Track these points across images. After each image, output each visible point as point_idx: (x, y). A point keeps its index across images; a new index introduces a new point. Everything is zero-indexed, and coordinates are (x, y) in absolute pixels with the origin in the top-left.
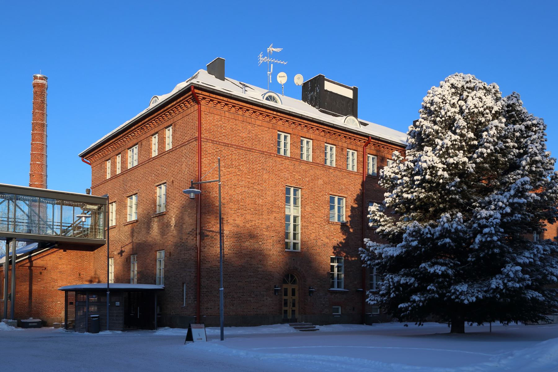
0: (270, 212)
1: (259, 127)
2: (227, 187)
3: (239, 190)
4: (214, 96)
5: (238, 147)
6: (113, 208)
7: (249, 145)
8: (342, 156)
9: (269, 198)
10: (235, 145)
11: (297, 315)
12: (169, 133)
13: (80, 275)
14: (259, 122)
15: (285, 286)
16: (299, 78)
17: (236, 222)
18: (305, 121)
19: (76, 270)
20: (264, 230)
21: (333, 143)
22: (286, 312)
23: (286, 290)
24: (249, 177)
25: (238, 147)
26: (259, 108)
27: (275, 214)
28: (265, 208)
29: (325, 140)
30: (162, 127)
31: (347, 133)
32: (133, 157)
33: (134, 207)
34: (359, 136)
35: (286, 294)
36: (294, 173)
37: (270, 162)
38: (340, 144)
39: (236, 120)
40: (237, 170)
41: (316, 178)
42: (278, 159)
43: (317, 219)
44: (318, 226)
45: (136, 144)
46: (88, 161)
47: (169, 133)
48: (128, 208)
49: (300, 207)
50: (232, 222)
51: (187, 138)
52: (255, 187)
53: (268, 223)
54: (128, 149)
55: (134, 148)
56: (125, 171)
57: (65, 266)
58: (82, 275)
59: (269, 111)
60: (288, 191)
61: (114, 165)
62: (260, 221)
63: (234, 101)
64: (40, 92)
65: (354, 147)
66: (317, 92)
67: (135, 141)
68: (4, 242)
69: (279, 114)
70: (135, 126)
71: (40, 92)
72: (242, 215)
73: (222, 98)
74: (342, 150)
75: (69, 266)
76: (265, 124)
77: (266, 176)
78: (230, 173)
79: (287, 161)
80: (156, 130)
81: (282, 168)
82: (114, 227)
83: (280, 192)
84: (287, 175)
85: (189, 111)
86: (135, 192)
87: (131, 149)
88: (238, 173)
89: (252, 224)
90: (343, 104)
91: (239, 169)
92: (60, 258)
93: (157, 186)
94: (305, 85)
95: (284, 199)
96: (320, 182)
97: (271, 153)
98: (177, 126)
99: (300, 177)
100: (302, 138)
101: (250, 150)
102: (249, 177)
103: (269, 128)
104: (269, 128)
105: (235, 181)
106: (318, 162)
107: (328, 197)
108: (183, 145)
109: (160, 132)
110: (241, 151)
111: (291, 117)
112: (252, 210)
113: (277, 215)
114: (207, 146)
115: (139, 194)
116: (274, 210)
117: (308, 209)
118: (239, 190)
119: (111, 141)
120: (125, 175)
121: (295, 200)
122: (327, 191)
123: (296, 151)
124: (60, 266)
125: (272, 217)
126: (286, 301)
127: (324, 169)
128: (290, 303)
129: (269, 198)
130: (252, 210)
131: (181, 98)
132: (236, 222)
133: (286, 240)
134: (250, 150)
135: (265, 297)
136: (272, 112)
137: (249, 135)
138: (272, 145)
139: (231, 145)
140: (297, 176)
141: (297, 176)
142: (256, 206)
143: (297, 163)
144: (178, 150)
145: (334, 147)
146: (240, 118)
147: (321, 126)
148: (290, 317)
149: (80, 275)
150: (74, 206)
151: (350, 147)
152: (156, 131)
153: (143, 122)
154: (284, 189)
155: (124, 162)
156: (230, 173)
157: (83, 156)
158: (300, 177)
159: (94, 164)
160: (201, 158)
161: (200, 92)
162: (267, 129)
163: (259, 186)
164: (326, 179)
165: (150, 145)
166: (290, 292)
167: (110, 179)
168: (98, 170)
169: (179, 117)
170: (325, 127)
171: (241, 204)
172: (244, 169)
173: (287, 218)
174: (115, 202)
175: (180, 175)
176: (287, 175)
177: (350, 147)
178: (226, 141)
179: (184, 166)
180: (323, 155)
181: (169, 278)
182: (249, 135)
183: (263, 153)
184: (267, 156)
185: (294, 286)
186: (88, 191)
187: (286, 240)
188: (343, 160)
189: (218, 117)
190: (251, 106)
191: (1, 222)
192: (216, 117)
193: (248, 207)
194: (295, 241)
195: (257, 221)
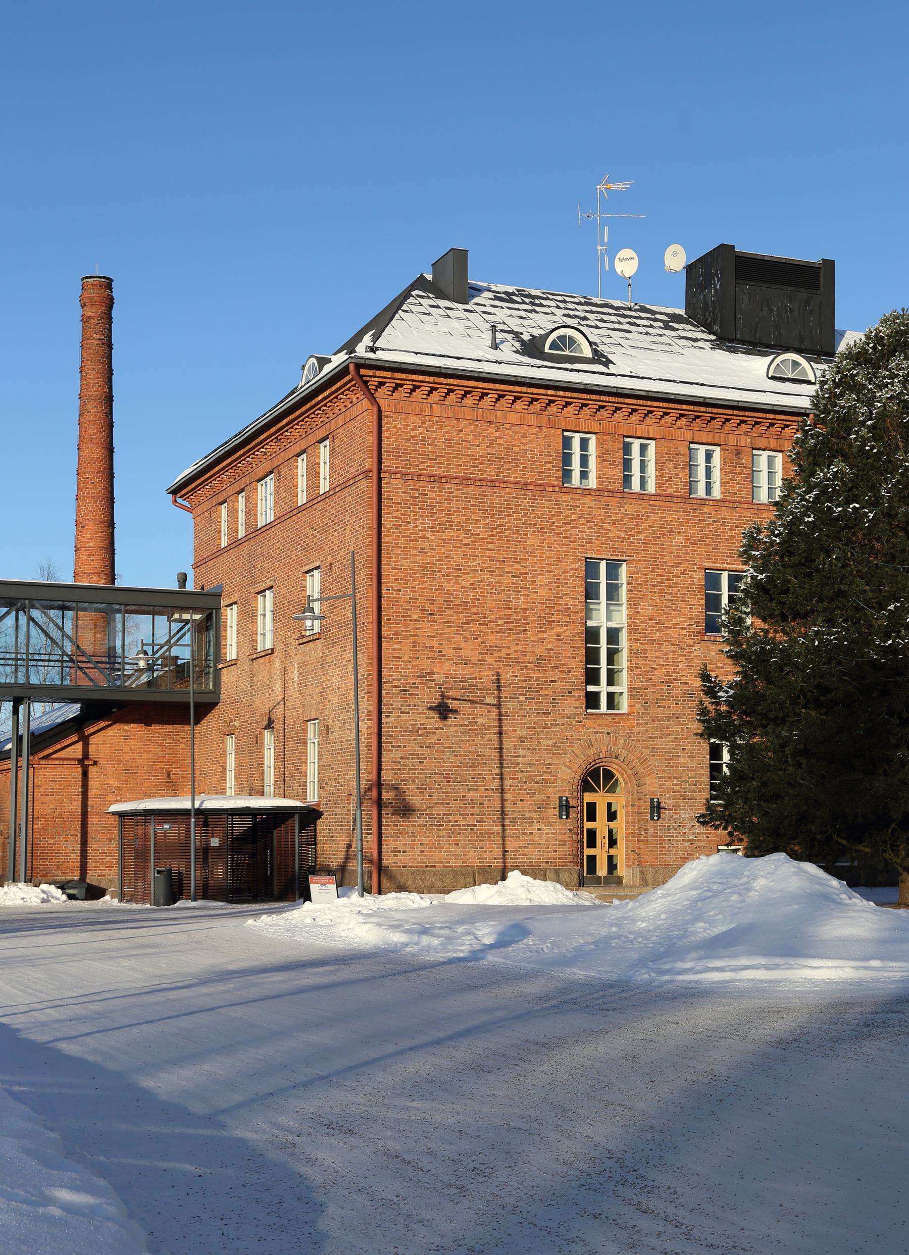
0: (546, 623)
1: (514, 429)
2: (439, 575)
3: (467, 579)
4: (403, 376)
5: (464, 481)
6: (231, 617)
7: (491, 473)
8: (738, 470)
9: (542, 592)
10: (457, 478)
11: (622, 870)
12: (324, 451)
13: (169, 776)
14: (513, 418)
15: (588, 797)
16: (675, 254)
17: (462, 653)
18: (628, 401)
19: (161, 765)
20: (530, 666)
21: (710, 441)
22: (592, 859)
23: (592, 807)
24: (491, 546)
25: (464, 481)
26: (511, 388)
27: (557, 629)
28: (532, 616)
29: (689, 436)
30: (312, 439)
31: (747, 413)
32: (266, 500)
33: (269, 615)
34: (782, 417)
35: (592, 817)
36: (606, 526)
37: (545, 506)
38: (732, 439)
39: (458, 420)
40: (462, 534)
41: (667, 531)
42: (565, 497)
43: (670, 631)
44: (672, 648)
45: (271, 472)
46: (186, 503)
47: (324, 451)
48: (259, 618)
49: (625, 607)
50: (452, 652)
51: (352, 470)
52: (507, 569)
53: (540, 650)
54: (259, 480)
55: (268, 479)
56: (255, 532)
57: (137, 756)
58: (173, 777)
59: (536, 391)
60: (591, 568)
61: (233, 513)
62: (520, 647)
63: (451, 381)
64: (101, 298)
65: (773, 444)
66: (716, 290)
67: (266, 466)
68: (8, 706)
69: (561, 393)
70: (265, 435)
71: (101, 298)
72: (476, 637)
73: (421, 378)
74: (738, 453)
75: (145, 755)
76: (530, 419)
77: (533, 541)
78: (446, 542)
79: (587, 500)
80: (303, 444)
81: (574, 517)
82: (234, 663)
83: (570, 573)
84: (588, 532)
85: (355, 411)
86: (269, 584)
87: (263, 482)
88: (465, 541)
89: (500, 654)
90: (791, 311)
91: (468, 532)
92: (126, 738)
93: (307, 572)
94: (689, 268)
95: (581, 589)
96: (678, 539)
97: (545, 486)
98: (337, 441)
99: (622, 534)
100: (627, 440)
101: (494, 484)
102: (491, 546)
103: (540, 427)
104: (540, 427)
105: (457, 558)
106: (670, 491)
107: (699, 577)
108: (345, 486)
109: (309, 451)
110: (471, 490)
111: (594, 397)
112: (500, 622)
113: (563, 629)
114: (391, 486)
115: (275, 587)
116: (555, 617)
117: (646, 609)
118: (467, 579)
119: (224, 463)
120: (252, 542)
121: (613, 592)
122: (697, 561)
123: (610, 471)
124: (126, 756)
125: (550, 635)
126: (592, 834)
127: (689, 507)
128: (602, 838)
129: (542, 592)
130: (500, 622)
131: (338, 385)
132: (462, 653)
133: (591, 688)
134: (494, 484)
135: (536, 826)
136: (543, 391)
137: (490, 451)
138: (549, 466)
139: (447, 477)
140: (614, 533)
141: (614, 533)
142: (510, 612)
143: (614, 502)
144: (338, 494)
145: (718, 449)
146: (469, 414)
147: (672, 406)
148: (602, 870)
149: (169, 776)
150: (154, 614)
151: (761, 443)
152: (303, 448)
153: (278, 426)
154: (581, 566)
155: (251, 512)
156: (446, 542)
157: (175, 491)
158: (622, 534)
159: (198, 510)
160: (380, 517)
161: (371, 373)
162: (534, 430)
163: (517, 566)
164: (691, 532)
165: (294, 477)
166: (601, 813)
167: (228, 549)
168: (206, 527)
169: (340, 421)
170: (685, 407)
171: (474, 610)
172: (480, 530)
173: (592, 635)
174: (235, 603)
175: (341, 553)
176: (588, 532)
177: (761, 443)
178: (435, 471)
179: (348, 532)
180: (684, 475)
181: (327, 784)
182: (490, 451)
183: (525, 486)
184: (538, 493)
185: (610, 797)
186: (183, 579)
187: (591, 688)
188: (740, 480)
189: (416, 419)
190: (491, 386)
191: (2, 662)
192: (412, 419)
193: (491, 617)
194: (612, 689)
195: (514, 648)
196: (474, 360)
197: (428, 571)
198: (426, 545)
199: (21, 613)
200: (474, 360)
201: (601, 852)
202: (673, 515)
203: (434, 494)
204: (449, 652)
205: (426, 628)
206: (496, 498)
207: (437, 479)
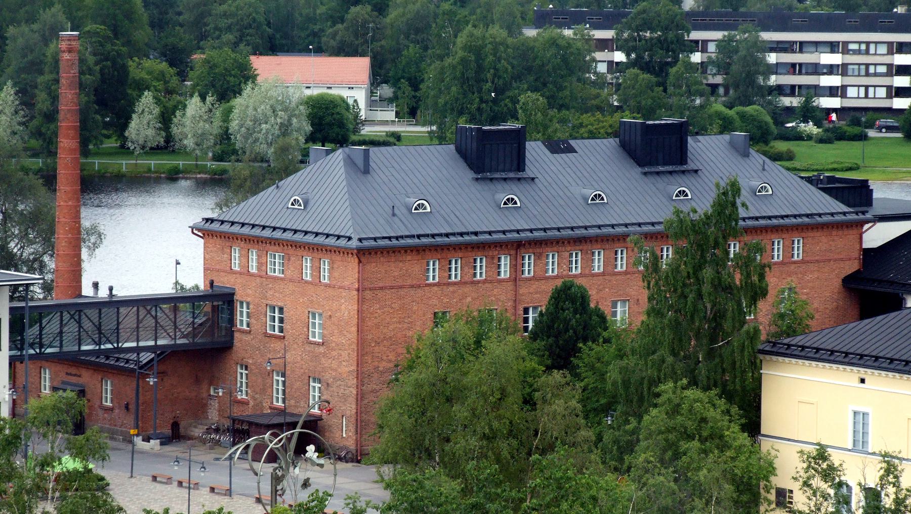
5: (392, 288)
25: (392, 288)
78: (384, 313)
84: (435, 301)
101: (401, 287)
134: (401, 287)
141: (445, 300)
172: (395, 306)
176: (435, 301)
178: (381, 285)
193: (400, 341)
196: (789, 440)
197: (377, 326)
198: (376, 315)
199: (141, 309)
200: (789, 440)
201: (277, 315)
202: (467, 289)
203: (380, 294)
204: (385, 358)
205: (377, 349)
206: (402, 292)
207: (381, 288)
